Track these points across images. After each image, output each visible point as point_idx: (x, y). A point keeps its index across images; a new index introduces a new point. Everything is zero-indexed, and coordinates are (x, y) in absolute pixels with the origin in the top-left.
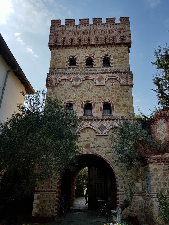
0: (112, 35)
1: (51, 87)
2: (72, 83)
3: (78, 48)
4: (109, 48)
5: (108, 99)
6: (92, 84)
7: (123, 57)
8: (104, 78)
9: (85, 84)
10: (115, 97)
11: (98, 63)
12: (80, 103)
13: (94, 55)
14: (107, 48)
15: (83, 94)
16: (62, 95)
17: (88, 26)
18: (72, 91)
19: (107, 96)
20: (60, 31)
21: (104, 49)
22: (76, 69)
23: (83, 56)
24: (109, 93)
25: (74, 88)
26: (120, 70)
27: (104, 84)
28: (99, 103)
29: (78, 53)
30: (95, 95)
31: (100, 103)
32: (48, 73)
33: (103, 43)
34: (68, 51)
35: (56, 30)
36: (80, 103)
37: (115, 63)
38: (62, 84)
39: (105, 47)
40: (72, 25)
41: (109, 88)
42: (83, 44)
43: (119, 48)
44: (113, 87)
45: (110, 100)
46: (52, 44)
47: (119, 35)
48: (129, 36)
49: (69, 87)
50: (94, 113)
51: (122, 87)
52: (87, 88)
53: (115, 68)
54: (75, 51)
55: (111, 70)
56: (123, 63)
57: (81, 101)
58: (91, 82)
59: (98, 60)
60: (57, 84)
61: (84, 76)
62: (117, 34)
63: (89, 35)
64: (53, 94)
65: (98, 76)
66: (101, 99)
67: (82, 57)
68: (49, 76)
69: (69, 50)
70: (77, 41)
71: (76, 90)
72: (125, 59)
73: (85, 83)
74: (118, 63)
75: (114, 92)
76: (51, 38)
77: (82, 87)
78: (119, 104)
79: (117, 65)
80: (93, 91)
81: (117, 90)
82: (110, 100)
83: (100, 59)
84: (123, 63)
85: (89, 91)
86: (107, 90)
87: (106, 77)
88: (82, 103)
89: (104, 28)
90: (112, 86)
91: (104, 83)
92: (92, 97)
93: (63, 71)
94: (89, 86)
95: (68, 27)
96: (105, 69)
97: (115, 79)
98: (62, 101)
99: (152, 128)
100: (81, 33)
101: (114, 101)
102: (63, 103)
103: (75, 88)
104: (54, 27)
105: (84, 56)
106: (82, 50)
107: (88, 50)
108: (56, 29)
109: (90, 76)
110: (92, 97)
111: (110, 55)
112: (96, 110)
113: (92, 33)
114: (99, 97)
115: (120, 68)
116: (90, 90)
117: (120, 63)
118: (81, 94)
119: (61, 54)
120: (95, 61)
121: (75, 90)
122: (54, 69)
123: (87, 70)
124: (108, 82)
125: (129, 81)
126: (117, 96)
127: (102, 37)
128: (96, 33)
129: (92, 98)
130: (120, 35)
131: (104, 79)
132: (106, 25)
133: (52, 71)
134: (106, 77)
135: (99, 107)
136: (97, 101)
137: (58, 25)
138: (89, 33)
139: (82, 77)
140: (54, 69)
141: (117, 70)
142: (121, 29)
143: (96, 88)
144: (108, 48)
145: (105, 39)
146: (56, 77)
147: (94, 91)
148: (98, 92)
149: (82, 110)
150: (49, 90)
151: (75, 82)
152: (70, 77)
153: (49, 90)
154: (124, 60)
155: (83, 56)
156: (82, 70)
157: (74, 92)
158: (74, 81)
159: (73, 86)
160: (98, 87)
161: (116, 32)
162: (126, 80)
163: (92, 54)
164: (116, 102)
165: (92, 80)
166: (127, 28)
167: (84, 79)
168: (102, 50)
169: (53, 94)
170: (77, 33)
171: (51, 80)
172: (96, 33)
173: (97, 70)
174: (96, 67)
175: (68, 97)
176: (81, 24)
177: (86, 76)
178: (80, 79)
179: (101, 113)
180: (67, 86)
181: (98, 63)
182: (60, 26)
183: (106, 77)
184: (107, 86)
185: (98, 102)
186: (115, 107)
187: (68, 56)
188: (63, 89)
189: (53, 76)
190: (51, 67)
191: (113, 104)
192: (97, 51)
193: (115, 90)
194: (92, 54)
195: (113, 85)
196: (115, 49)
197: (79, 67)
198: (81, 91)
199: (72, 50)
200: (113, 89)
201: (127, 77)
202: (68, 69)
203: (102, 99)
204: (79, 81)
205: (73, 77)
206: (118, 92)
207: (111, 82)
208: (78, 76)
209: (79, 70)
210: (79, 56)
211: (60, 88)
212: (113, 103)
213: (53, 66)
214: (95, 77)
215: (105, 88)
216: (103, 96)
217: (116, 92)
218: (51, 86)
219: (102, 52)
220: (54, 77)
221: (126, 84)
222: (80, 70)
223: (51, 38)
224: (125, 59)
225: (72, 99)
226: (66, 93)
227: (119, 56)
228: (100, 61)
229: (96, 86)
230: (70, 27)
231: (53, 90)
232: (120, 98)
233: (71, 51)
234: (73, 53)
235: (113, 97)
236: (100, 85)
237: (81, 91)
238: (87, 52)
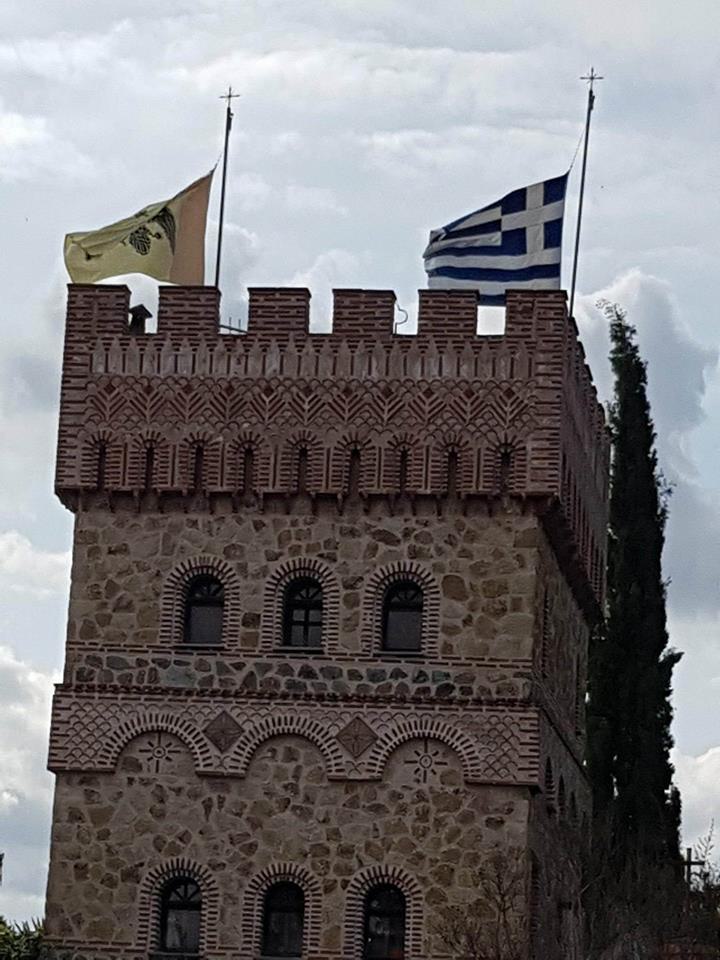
0: (445, 428)
1: (76, 779)
2: (198, 756)
3: (235, 510)
4: (424, 518)
5: (394, 863)
6: (312, 767)
7: (503, 589)
8: (380, 734)
9: (272, 763)
10: (432, 856)
11: (350, 624)
12: (241, 886)
13: (333, 567)
14: (414, 519)
15: (255, 825)
16: (143, 828)
17: (300, 348)
18: (198, 805)
19: (388, 849)
20: (124, 381)
21: (394, 525)
22: (219, 658)
23: (264, 571)
24: (400, 827)
25: (205, 784)
26: (477, 679)
27: (375, 774)
28: (344, 888)
29: (234, 541)
30: (325, 836)
31: (350, 888)
32: (56, 685)
33: (384, 491)
34: (175, 529)
35: (101, 369)
36: (241, 886)
37: (450, 630)
38: (142, 758)
39: (401, 511)
40: (200, 334)
41: (406, 793)
42: (266, 490)
43: (484, 520)
44: (427, 792)
45: (401, 871)
46: (76, 482)
47: (491, 435)
48: (547, 444)
49: (181, 782)
50: (313, 948)
51: (477, 792)
52: (278, 787)
53: (450, 662)
54: (215, 526)
55: (421, 676)
56: (495, 631)
57: (245, 871)
58: (302, 752)
59: (351, 602)
60: (108, 762)
61: (263, 712)
62: (479, 422)
63: (306, 423)
64: (87, 817)
65: (347, 715)
66: (354, 862)
67: (256, 576)
68: (65, 702)
69: (183, 518)
70: (228, 469)
71: (219, 797)
72: (509, 605)
73: (269, 754)
74: (468, 628)
75: (432, 820)
76: (71, 431)
77: (251, 781)
78: (450, 899)
79: (464, 641)
80: (311, 813)
81: (446, 809)
82: (401, 871)
83: (362, 595)
84: (495, 631)
85: (288, 812)
86: (393, 810)
87: (392, 725)
88: (251, 886)
89: (397, 372)
90: (424, 787)
91: (378, 769)
92: (307, 847)
93: (147, 669)
94: (292, 781)
95: (176, 346)
96: (389, 667)
97: (437, 740)
98: (142, 865)
99: (564, 916)
100: (257, 406)
101: (423, 880)
102: (144, 881)
103: (213, 787)
104: (86, 349)
105: (274, 567)
106: (258, 526)
107: (294, 523)
108: (102, 360)
109: (300, 716)
110: (307, 847)
111: (424, 566)
112: (325, 927)
113: (327, 407)
114: (345, 852)
115: (474, 663)
116: (298, 801)
117: (480, 633)
118: (247, 828)
119: (132, 546)
120: (335, 606)
121: (210, 799)
122: (91, 653)
123: (286, 670)
124: (398, 755)
125: (515, 758)
126: (444, 849)
127: (382, 441)
128: (347, 408)
129: (306, 855)
130: (492, 430)
131: (379, 742)
132: (505, 346)
133: (82, 664)
134: (392, 725)
135: (343, 914)
136: (332, 876)
137: (110, 327)
138: (306, 407)
139: (251, 719)
140: (91, 653)
141: (458, 679)
142: (505, 386)
143: (332, 793)
144: (417, 522)
145: (404, 454)
146: (107, 715)
147: (319, 810)
148: (342, 821)
149: (247, 928)
150: (66, 794)
151: (214, 751)
152: (186, 717)
153: (66, 794)
154: (504, 610)
155: (265, 564)
156: (254, 669)
157: (208, 806)
158: (211, 746)
159: (202, 775)
160: (341, 789)
161: (468, 408)
162: (499, 753)
163: (321, 556)
164: (437, 886)
165: (312, 742)
166: (540, 379)
167: (263, 734)
168: (380, 532)
169: (87, 817)
170: (230, 399)
171: (85, 728)
172: (347, 408)
173: (345, 673)
174: (340, 649)
175: (173, 843)
176: (259, 334)
177: (279, 713)
178: (243, 731)
179: (348, 858)
180: (164, 769)
181: (350, 624)
182: (143, 334)
183: (389, 725)
184: (394, 783)
185: (339, 879)
186: (425, 915)
187: (177, 564)
188: (147, 791)
189: (87, 709)
190: (77, 638)
191: (421, 899)
192: (353, 533)
193: (433, 808)
194: (320, 561)
195: (430, 775)
196: (460, 527)
197: (240, 647)
198: (247, 810)
199: (202, 518)
200: (422, 804)
201: (507, 735)
202: (173, 657)
203: (361, 864)
204: (238, 743)
205: (200, 719)
206: (452, 821)
207: (418, 759)
208: (234, 714)
209: (239, 666)
210: (243, 568)
211: (131, 781)
212: (419, 892)
213: (89, 631)
214: (331, 722)
215: (382, 797)
216: (368, 845)
217: (439, 823)
218: (78, 771)
219: (383, 547)
220: (94, 714)
221: (497, 779)
222: (244, 665)
223: (71, 431)
224: (509, 605)
225: (194, 855)
226: (160, 815)
227: (479, 582)
228: (361, 608)
229: (330, 780)
230: (185, 349)
231: (89, 794)
232: (461, 860)
233: (195, 523)
234: (206, 539)
235: (421, 857)
236: (351, 777)
237: (245, 806)
238: (290, 539)
